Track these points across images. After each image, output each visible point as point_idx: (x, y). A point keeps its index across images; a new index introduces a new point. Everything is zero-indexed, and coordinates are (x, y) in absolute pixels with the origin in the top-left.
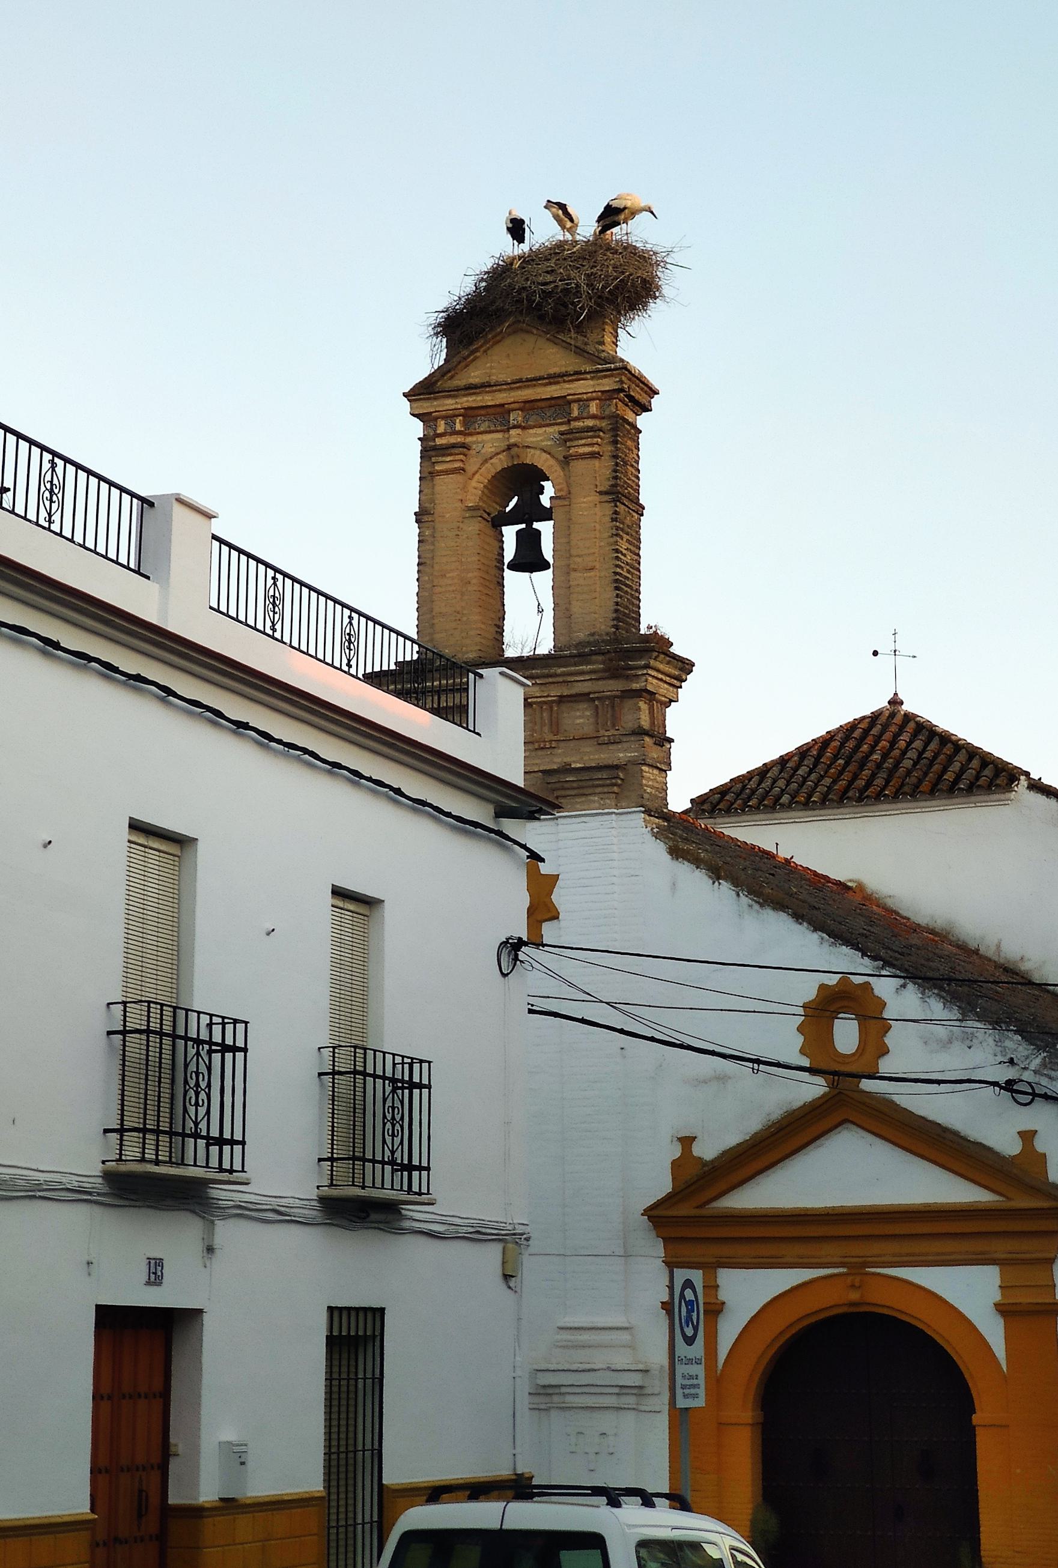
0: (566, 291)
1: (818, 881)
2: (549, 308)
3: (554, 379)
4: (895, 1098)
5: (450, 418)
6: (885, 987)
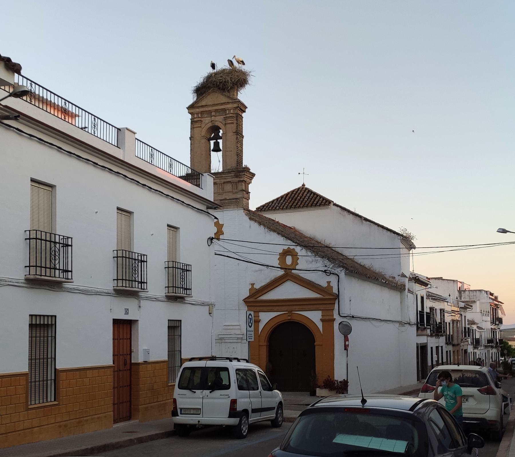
0: (225, 82)
1: (285, 226)
2: (221, 86)
3: (222, 104)
4: (300, 274)
5: (197, 114)
6: (298, 249)
